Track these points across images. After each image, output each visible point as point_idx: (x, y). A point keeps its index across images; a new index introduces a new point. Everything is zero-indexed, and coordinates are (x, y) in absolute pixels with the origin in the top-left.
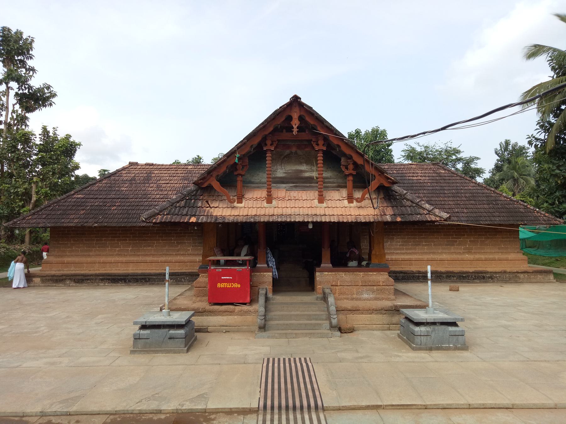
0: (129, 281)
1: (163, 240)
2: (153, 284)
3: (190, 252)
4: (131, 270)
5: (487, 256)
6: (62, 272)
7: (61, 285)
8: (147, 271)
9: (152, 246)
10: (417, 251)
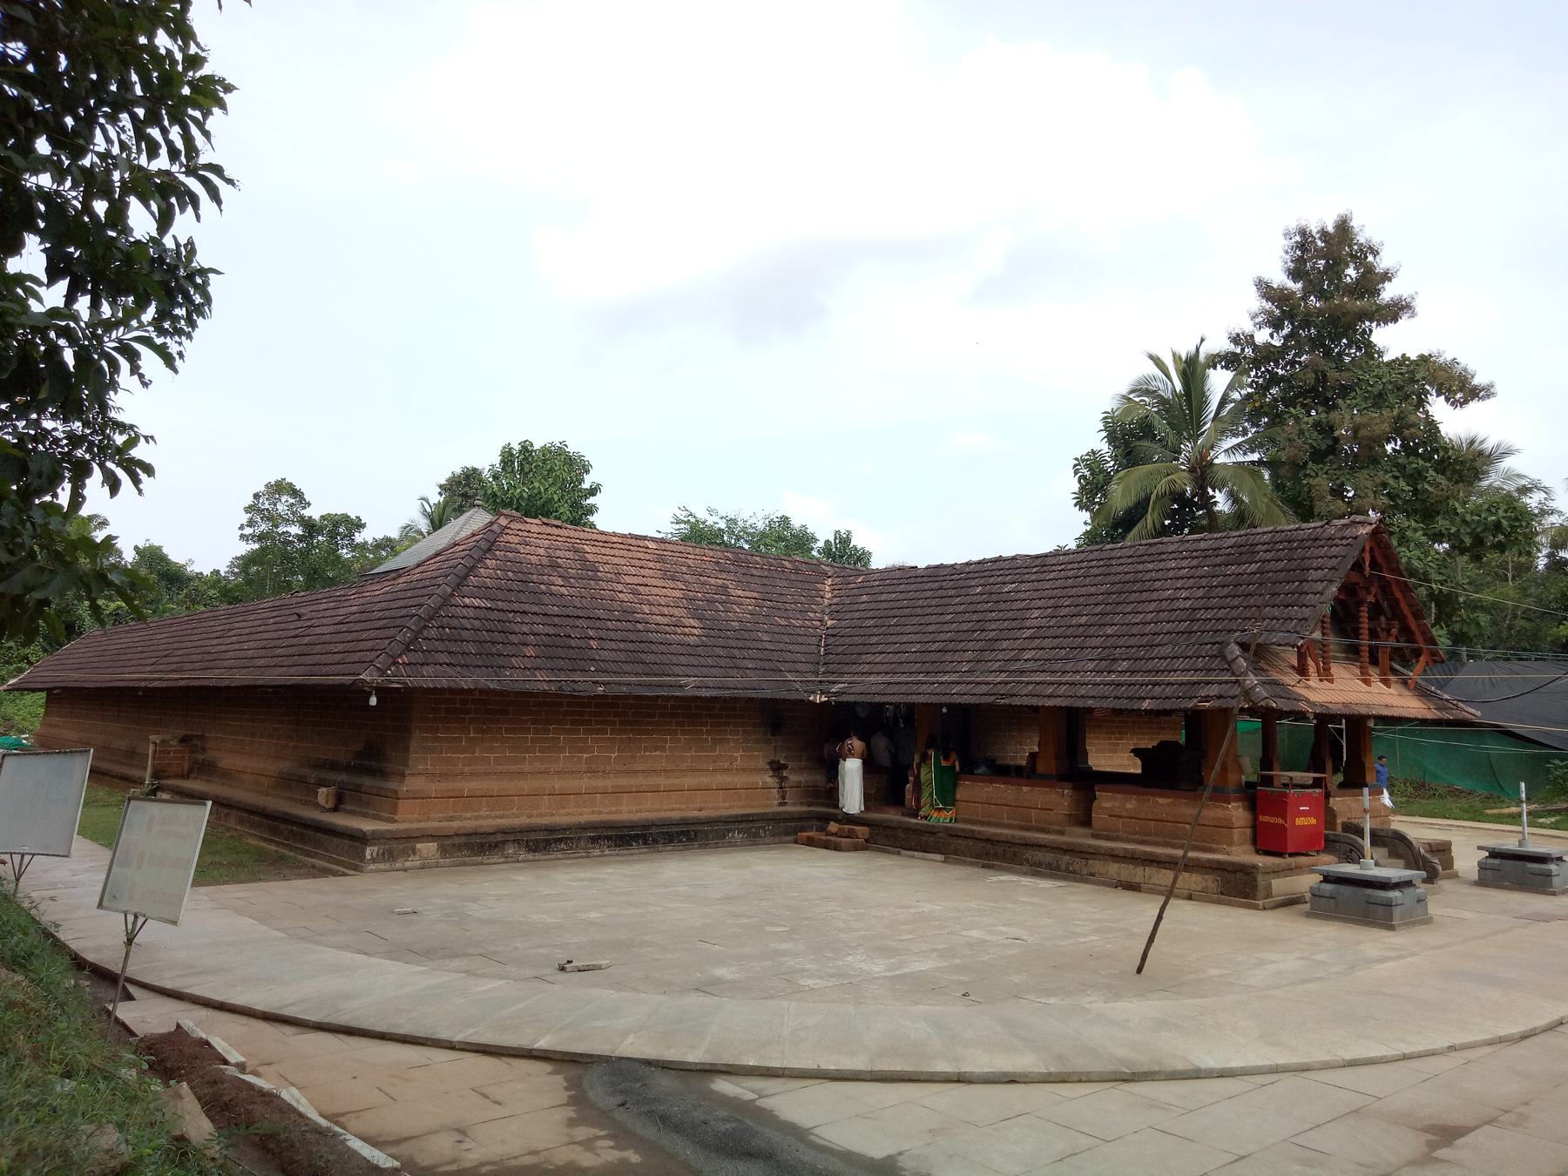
0: (655, 841)
1: (684, 733)
2: (706, 846)
3: (739, 763)
4: (627, 811)
5: (669, 781)
6: (456, 824)
7: (495, 859)
8: (662, 815)
9: (663, 749)
10: (526, 767)
